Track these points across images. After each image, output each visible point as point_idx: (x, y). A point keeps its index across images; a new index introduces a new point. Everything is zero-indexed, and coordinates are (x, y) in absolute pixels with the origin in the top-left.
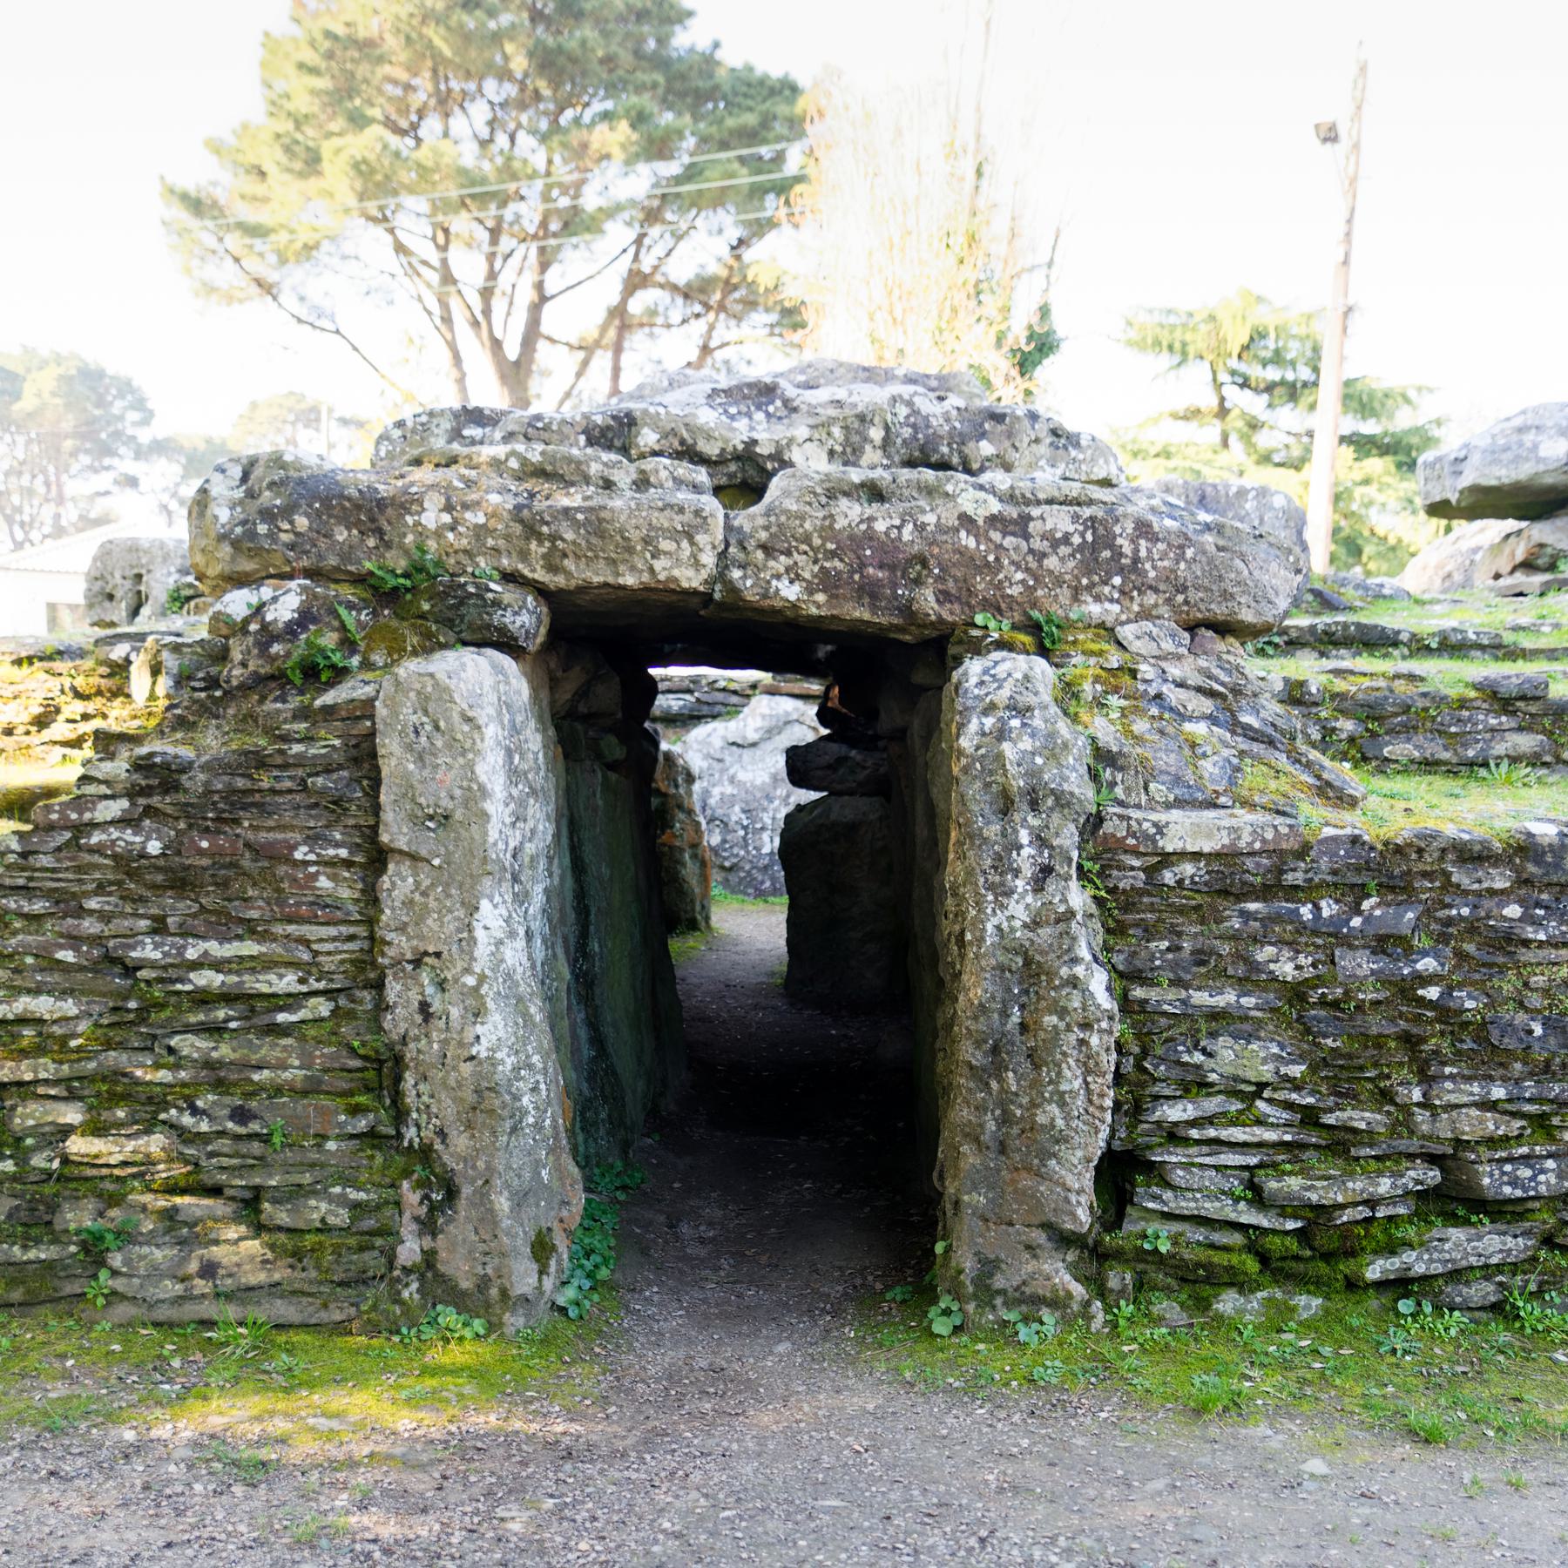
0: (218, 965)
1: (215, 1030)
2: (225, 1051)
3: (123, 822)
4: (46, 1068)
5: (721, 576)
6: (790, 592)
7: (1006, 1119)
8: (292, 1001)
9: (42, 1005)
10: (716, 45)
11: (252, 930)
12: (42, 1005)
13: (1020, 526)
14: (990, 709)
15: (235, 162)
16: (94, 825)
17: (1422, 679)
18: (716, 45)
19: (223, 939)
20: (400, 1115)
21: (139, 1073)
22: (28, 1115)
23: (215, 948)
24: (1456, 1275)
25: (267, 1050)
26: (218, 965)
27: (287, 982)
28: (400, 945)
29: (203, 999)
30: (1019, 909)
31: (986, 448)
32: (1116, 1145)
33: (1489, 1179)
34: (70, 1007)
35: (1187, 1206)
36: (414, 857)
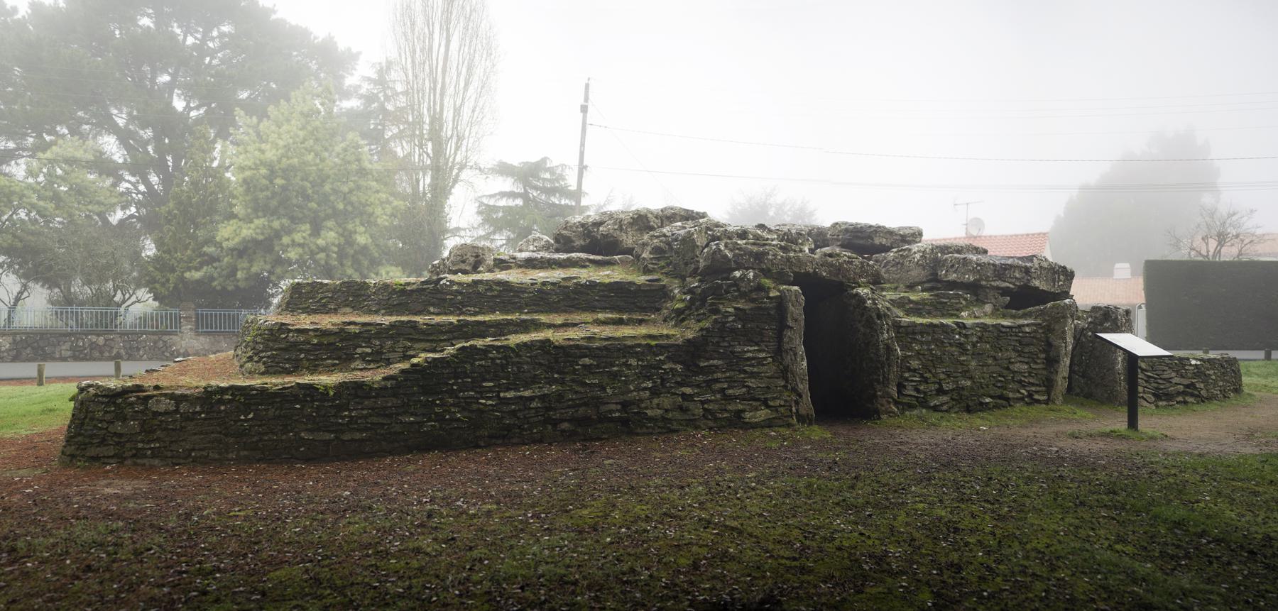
0: (751, 351)
1: (753, 366)
2: (755, 370)
3: (733, 321)
4: (719, 375)
5: (815, 270)
6: (824, 274)
7: (884, 377)
8: (765, 358)
9: (715, 362)
10: (275, 5)
11: (757, 344)
12: (715, 362)
13: (851, 263)
14: (869, 299)
15: (390, 64)
16: (728, 322)
17: (985, 252)
18: (275, 5)
19: (751, 346)
20: (787, 382)
21: (1070, 347)
22: (717, 386)
23: (750, 348)
24: (942, 405)
25: (764, 369)
26: (751, 351)
27: (764, 355)
28: (786, 346)
29: (749, 359)
30: (886, 336)
31: (800, 241)
32: (1242, 364)
33: (945, 387)
34: (720, 362)
35: (909, 393)
36: (792, 328)
